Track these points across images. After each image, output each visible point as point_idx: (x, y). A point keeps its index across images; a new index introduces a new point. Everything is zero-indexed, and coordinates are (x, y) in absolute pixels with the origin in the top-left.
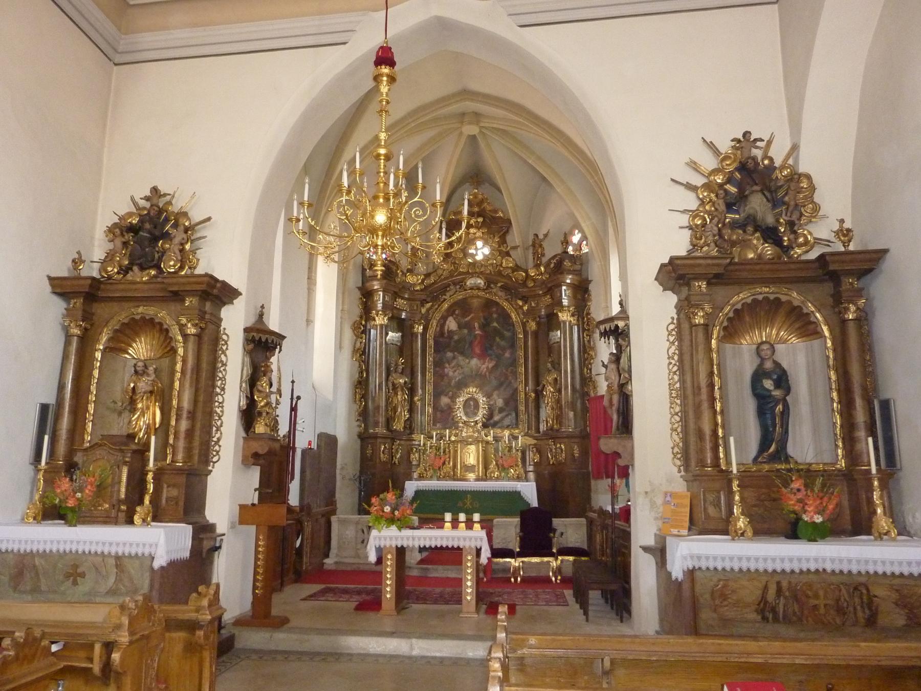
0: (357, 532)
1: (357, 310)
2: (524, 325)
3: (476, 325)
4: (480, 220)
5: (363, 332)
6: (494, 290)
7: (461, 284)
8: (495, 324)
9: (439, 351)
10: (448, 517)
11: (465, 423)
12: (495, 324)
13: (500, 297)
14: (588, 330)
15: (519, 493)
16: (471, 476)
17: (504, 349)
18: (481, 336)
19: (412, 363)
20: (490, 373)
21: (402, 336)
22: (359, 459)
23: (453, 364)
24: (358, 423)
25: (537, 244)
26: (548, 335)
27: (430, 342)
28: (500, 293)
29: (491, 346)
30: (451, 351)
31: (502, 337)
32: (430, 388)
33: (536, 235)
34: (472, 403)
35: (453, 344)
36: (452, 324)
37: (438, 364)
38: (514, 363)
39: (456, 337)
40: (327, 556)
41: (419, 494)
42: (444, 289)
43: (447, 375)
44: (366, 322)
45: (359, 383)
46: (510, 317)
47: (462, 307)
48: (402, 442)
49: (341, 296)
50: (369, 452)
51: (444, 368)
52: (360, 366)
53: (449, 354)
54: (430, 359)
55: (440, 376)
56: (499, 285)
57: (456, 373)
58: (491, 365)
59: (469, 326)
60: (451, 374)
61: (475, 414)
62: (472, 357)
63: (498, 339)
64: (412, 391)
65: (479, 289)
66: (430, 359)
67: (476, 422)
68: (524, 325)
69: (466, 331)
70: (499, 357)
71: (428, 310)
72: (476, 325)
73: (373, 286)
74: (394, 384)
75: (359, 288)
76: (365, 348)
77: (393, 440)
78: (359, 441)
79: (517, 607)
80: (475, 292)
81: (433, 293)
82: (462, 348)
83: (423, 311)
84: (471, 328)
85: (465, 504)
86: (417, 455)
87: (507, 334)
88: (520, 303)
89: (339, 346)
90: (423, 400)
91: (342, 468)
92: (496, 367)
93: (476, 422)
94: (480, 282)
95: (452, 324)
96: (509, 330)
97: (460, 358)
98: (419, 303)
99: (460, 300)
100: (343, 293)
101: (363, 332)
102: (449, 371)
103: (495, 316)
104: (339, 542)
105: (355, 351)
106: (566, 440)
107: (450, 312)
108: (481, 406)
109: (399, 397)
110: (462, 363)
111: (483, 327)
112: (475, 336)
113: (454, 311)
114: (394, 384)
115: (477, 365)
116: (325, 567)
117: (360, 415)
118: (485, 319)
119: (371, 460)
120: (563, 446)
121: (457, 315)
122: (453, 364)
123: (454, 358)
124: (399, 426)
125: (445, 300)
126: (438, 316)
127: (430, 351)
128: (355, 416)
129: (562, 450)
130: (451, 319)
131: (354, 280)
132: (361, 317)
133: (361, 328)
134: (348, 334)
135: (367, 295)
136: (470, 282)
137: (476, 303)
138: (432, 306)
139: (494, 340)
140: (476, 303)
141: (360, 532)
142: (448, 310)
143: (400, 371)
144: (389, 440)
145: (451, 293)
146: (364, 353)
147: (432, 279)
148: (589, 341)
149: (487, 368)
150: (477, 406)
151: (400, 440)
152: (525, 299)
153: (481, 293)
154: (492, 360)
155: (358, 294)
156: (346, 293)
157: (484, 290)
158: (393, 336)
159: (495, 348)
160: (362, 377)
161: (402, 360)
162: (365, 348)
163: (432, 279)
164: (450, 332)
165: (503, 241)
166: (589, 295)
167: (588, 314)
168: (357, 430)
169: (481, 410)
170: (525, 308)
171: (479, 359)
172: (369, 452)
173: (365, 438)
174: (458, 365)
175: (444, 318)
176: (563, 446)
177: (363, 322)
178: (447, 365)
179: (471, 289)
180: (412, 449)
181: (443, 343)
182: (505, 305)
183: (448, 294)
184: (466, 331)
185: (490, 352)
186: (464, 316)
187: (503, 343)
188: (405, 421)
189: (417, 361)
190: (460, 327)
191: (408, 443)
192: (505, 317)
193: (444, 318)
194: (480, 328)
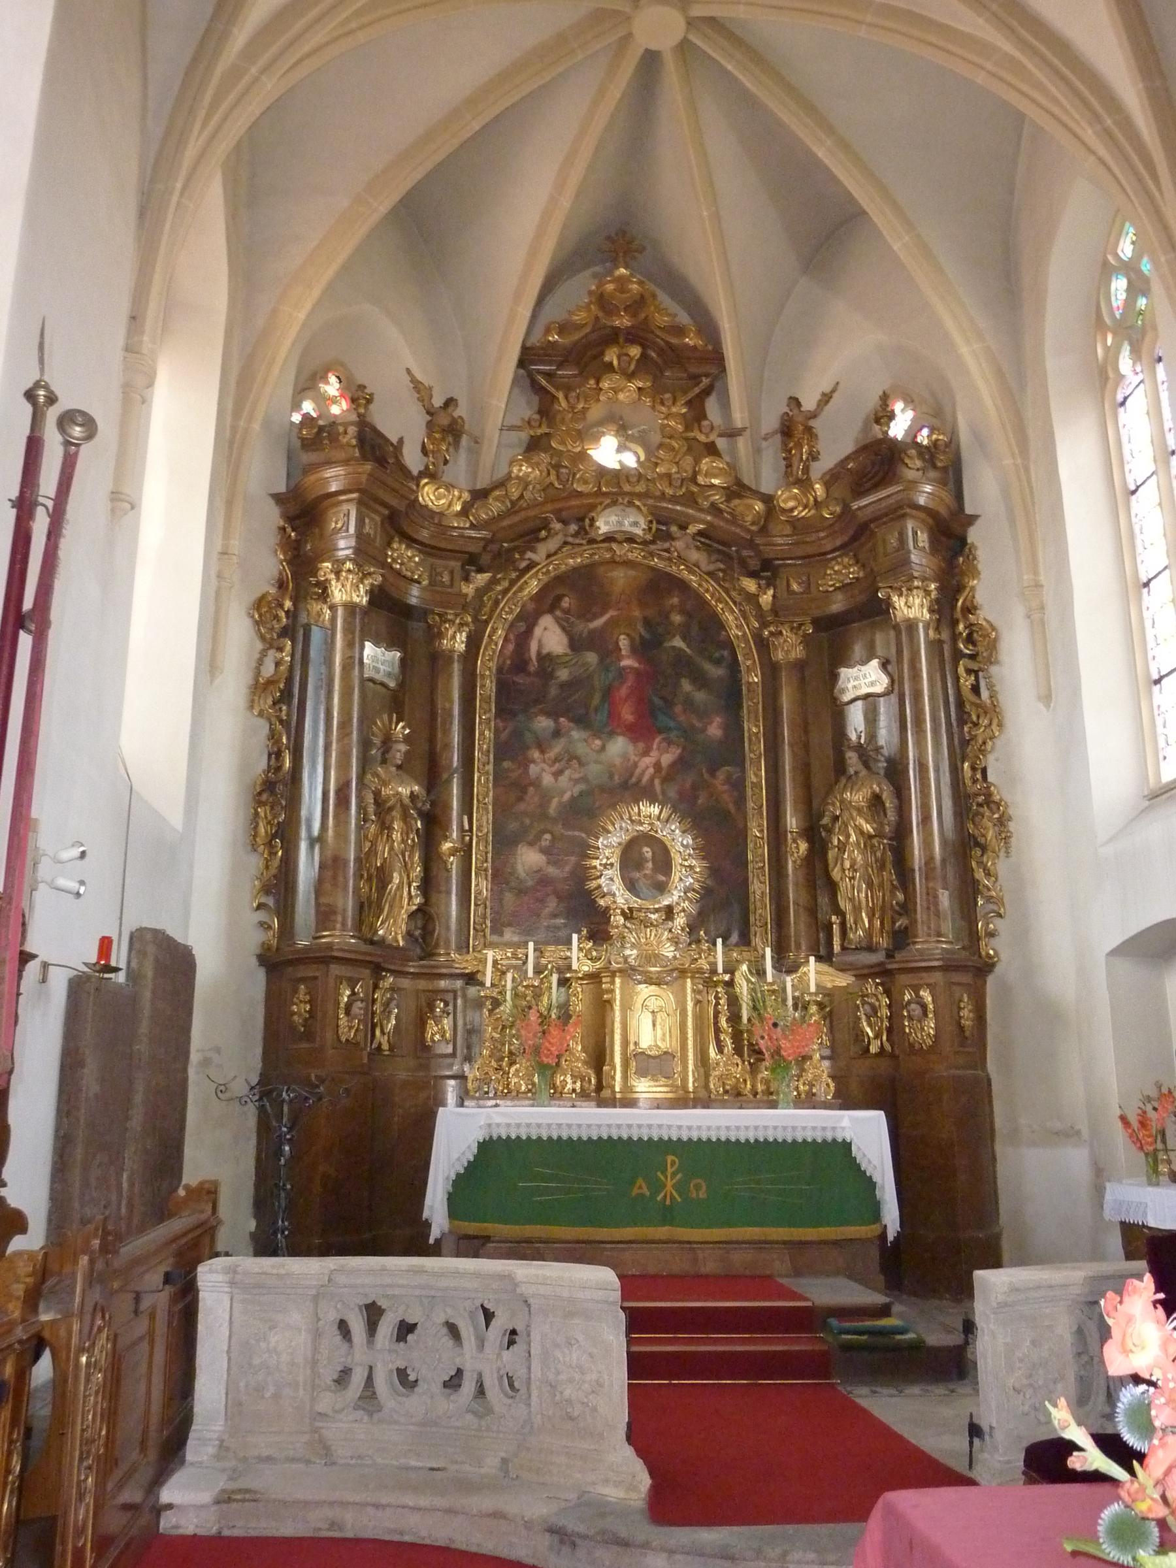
0: (317, 1334)
1: (268, 565)
2: (763, 646)
3: (624, 642)
4: (635, 351)
5: (286, 632)
6: (679, 544)
7: (583, 520)
8: (678, 642)
9: (513, 714)
10: (1161, 1296)
11: (628, 915)
12: (678, 642)
13: (691, 564)
14: (973, 657)
15: (847, 1146)
16: (644, 1088)
17: (704, 714)
18: (638, 673)
19: (432, 740)
20: (664, 780)
21: (403, 661)
22: (259, 1034)
23: (552, 754)
24: (261, 916)
25: (794, 430)
26: (834, 677)
27: (487, 687)
28: (695, 556)
29: (669, 703)
30: (548, 714)
31: (701, 681)
32: (483, 820)
33: (795, 402)
34: (647, 852)
35: (553, 691)
36: (550, 637)
37: (510, 749)
38: (731, 750)
39: (563, 674)
40: (172, 1448)
41: (493, 1152)
42: (531, 535)
43: (537, 783)
44: (296, 600)
45: (269, 786)
46: (721, 626)
47: (578, 591)
48: (405, 983)
49: (220, 504)
50: (300, 1008)
51: (526, 763)
52: (273, 736)
53: (543, 723)
54: (485, 736)
55: (513, 787)
56: (692, 529)
57: (563, 780)
58: (667, 759)
59: (600, 643)
60: (547, 780)
61: (662, 888)
62: (612, 734)
63: (686, 686)
64: (433, 823)
65: (631, 539)
66: (485, 736)
67: (669, 912)
68: (763, 646)
69: (592, 658)
70: (688, 735)
71: (481, 592)
72: (624, 642)
73: (326, 481)
74: (379, 801)
75: (278, 498)
76: (289, 681)
77: (378, 970)
78: (261, 975)
79: (625, 1478)
80: (621, 550)
81: (503, 545)
82: (579, 706)
83: (469, 590)
84: (608, 653)
85: (657, 1187)
86: (447, 1023)
87: (716, 672)
88: (750, 585)
89: (209, 663)
90: (465, 851)
91: (206, 1062)
92: (681, 764)
93: (669, 912)
94: (634, 522)
95: (550, 637)
96: (718, 662)
97: (576, 734)
98: (456, 565)
99: (575, 569)
100: (229, 503)
101: (286, 632)
102: (541, 769)
103: (677, 618)
104: (230, 1387)
105: (259, 687)
106: (937, 977)
107: (546, 601)
108: (677, 859)
109: (397, 836)
110: (581, 749)
111: (643, 648)
112: (622, 673)
113: (559, 598)
114: (379, 801)
115: (625, 756)
116: (168, 1523)
117: (266, 890)
118: (647, 623)
119: (309, 1036)
120: (926, 995)
121: (567, 612)
122: (552, 754)
123: (557, 734)
124: (393, 928)
125: (532, 565)
126: (508, 612)
127: (484, 717)
128: (248, 895)
129: (924, 1007)
130: (547, 621)
131: (265, 473)
132: (281, 585)
133: (286, 613)
134: (240, 634)
135: (302, 515)
136: (605, 524)
137: (620, 579)
138: (493, 582)
139: (677, 685)
140: (620, 579)
141: (332, 1336)
142: (538, 597)
143: (398, 758)
144: (367, 972)
145: (552, 544)
146: (286, 696)
147: (494, 506)
148: (976, 689)
149: (657, 766)
150: (664, 863)
151: (398, 973)
152: (767, 570)
153: (636, 555)
154: (670, 743)
155: (273, 516)
156: (238, 511)
157: (645, 543)
158: (378, 658)
159: (678, 709)
160: (279, 769)
161: (401, 729)
162: (289, 681)
163: (494, 506)
164: (546, 659)
165: (697, 415)
166: (971, 558)
167: (970, 609)
168: (254, 939)
169: (676, 876)
170: (766, 599)
171: (634, 741)
172: (300, 1008)
173: (280, 963)
174: (572, 757)
175: (527, 621)
176: (926, 995)
177: (288, 604)
178: (536, 754)
179: (609, 538)
180: (431, 1007)
181: (524, 688)
182: (709, 590)
183: (543, 549)
184: (592, 658)
185: (663, 720)
186: (586, 614)
187: (700, 696)
188: (412, 916)
189: (447, 732)
190: (576, 644)
191: (422, 984)
192: (708, 628)
193: (527, 621)
194: (634, 650)
